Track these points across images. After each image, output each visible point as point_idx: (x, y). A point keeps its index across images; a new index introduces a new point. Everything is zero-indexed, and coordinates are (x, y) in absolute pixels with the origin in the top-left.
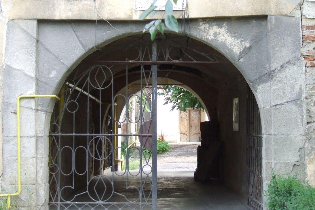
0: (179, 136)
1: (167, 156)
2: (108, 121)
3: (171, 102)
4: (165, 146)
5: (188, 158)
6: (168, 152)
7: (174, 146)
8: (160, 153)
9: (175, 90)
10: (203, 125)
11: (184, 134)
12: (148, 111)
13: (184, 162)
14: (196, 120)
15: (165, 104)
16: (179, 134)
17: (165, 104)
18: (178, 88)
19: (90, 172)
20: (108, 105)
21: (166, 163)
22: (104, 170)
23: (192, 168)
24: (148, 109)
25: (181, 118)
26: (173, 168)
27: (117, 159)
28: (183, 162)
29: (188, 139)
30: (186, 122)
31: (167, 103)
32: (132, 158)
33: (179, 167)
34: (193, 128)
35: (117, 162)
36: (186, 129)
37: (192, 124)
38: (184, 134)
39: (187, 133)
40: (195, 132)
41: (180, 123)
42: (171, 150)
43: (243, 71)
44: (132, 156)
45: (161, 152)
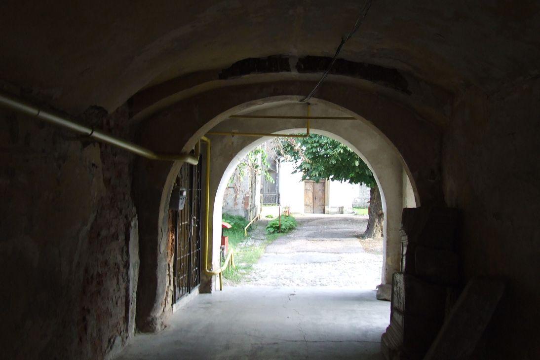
0: (303, 207)
1: (294, 239)
2: (178, 199)
3: (301, 171)
4: (292, 223)
5: (322, 243)
6: (295, 231)
7: (301, 220)
8: (286, 233)
9: (308, 153)
10: (407, 212)
11: (308, 205)
12: (271, 181)
13: (320, 252)
14: (320, 192)
15: (293, 173)
16: (304, 206)
17: (293, 173)
18: (312, 151)
19: (109, 341)
20: (174, 162)
21: (295, 253)
22: (174, 305)
23: (333, 263)
24: (271, 178)
25: (306, 190)
26: (306, 264)
27: (210, 270)
28: (318, 252)
29: (312, 211)
30: (310, 195)
31: (295, 172)
32: (253, 238)
33: (314, 261)
34: (317, 201)
35: (210, 276)
36: (311, 201)
37: (317, 195)
38: (308, 205)
39: (312, 205)
40: (319, 204)
41: (305, 195)
42: (298, 227)
43: (230, 211)
44: (253, 237)
45: (287, 231)
